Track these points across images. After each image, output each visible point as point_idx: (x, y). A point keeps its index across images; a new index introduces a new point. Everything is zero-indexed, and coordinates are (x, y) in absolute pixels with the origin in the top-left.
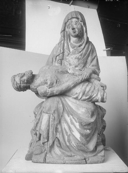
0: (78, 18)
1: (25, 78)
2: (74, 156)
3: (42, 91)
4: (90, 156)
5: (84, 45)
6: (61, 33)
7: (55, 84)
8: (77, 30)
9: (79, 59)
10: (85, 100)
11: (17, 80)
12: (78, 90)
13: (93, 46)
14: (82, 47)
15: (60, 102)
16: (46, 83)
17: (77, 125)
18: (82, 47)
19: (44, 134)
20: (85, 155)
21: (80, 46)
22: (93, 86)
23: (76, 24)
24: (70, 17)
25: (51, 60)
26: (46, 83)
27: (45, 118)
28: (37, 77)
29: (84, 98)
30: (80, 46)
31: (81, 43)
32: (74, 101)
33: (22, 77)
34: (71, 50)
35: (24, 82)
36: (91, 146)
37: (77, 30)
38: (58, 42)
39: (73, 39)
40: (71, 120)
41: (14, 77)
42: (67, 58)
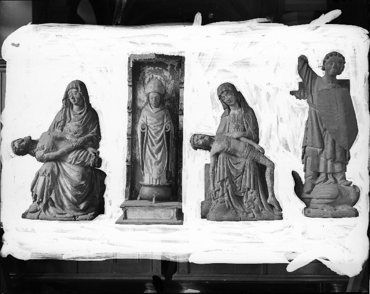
0: (77, 89)
1: (24, 143)
2: (65, 214)
3: (155, 176)
4: (80, 214)
5: (84, 114)
6: (63, 101)
7: (50, 150)
8: (76, 100)
9: (79, 126)
10: (77, 165)
11: (16, 145)
12: (72, 156)
13: (306, 66)
14: (83, 115)
15: (56, 167)
16: (43, 149)
17: (69, 186)
18: (83, 115)
19: (38, 194)
20: (76, 214)
21: (80, 114)
22: (86, 153)
23: (76, 94)
24: (71, 87)
25: (53, 126)
26: (43, 149)
27: (41, 179)
28: (235, 148)
29: (77, 163)
30: (80, 114)
31: (81, 111)
32: (69, 165)
33: (21, 143)
34: (72, 117)
35: (22, 146)
36: (82, 206)
37: (76, 100)
38: (60, 109)
39: (75, 107)
40: (64, 182)
41: (14, 142)
42: (68, 124)
